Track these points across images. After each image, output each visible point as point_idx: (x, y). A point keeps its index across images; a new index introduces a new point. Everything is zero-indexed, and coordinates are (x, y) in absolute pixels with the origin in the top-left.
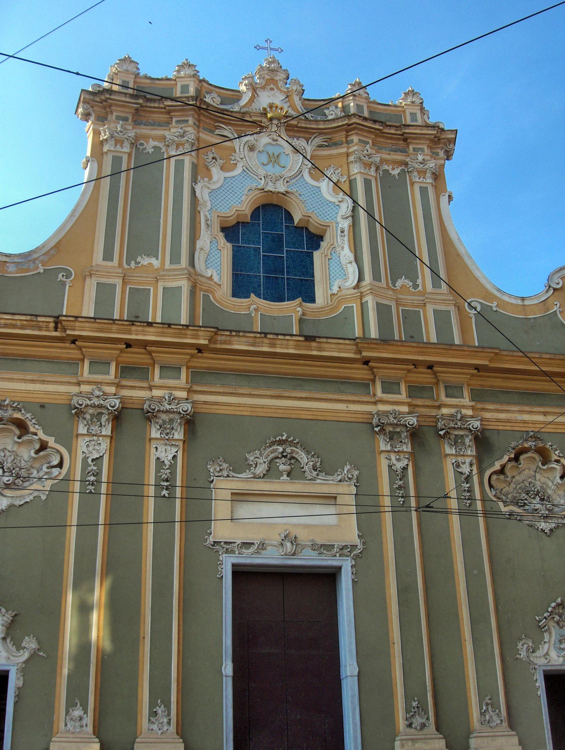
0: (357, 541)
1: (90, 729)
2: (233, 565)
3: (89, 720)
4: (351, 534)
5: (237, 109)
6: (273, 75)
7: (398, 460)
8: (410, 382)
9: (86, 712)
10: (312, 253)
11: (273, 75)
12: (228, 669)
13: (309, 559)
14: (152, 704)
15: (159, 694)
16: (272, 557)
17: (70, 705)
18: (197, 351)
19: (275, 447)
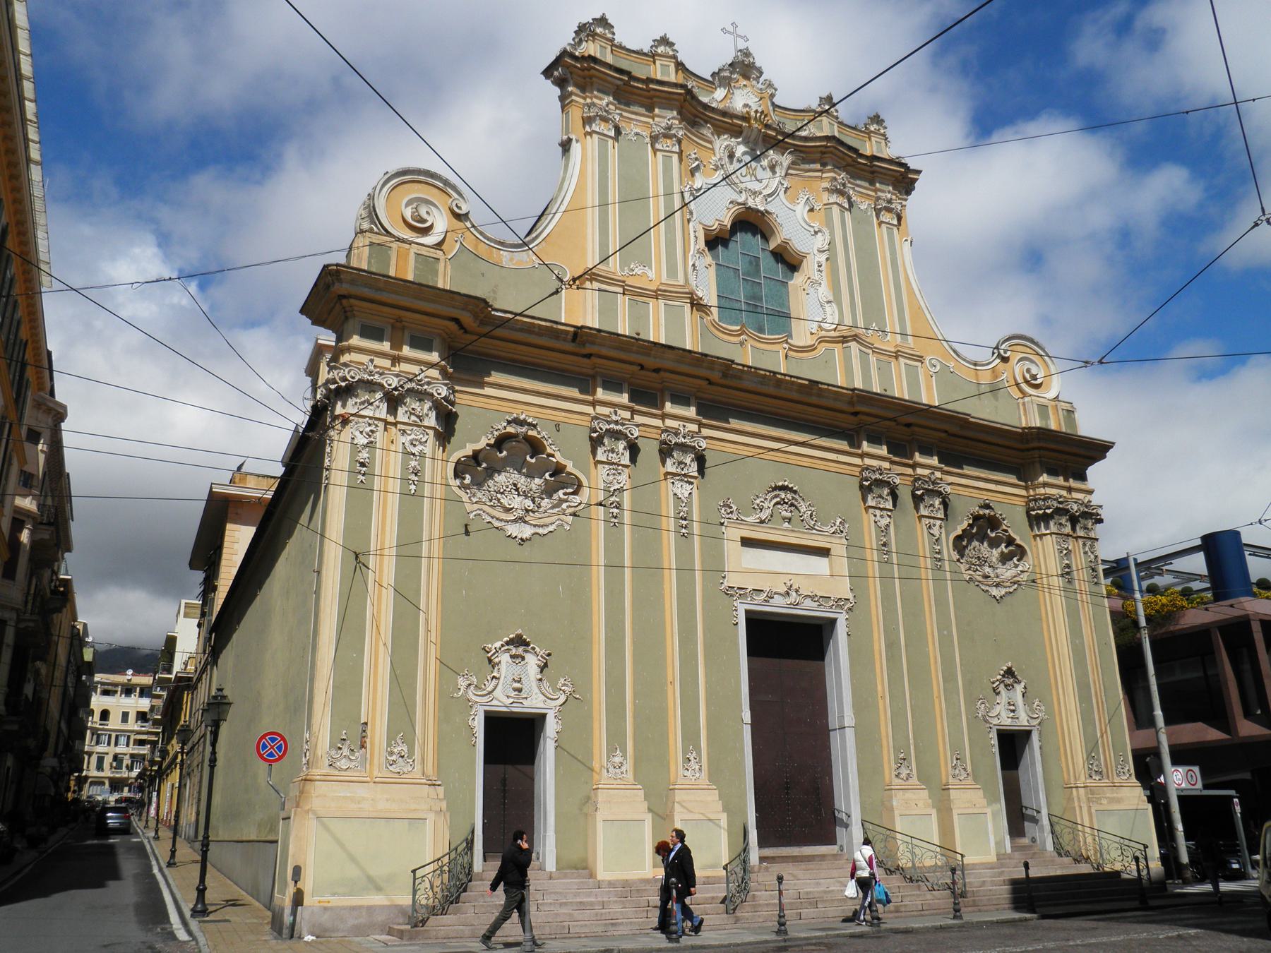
0: (850, 596)
1: (630, 776)
2: (747, 612)
3: (628, 766)
4: (842, 589)
5: (705, 99)
6: (744, 68)
7: (882, 516)
8: (701, 398)
9: (625, 759)
10: (1206, 787)
11: (744, 68)
12: (747, 717)
13: (809, 609)
14: (685, 752)
15: (691, 738)
16: (779, 606)
17: (611, 752)
18: (193, 287)
19: (777, 492)
